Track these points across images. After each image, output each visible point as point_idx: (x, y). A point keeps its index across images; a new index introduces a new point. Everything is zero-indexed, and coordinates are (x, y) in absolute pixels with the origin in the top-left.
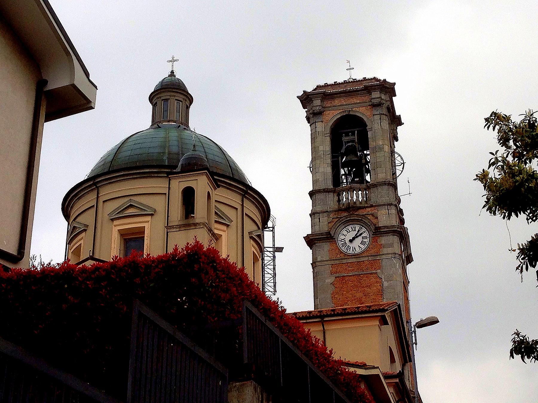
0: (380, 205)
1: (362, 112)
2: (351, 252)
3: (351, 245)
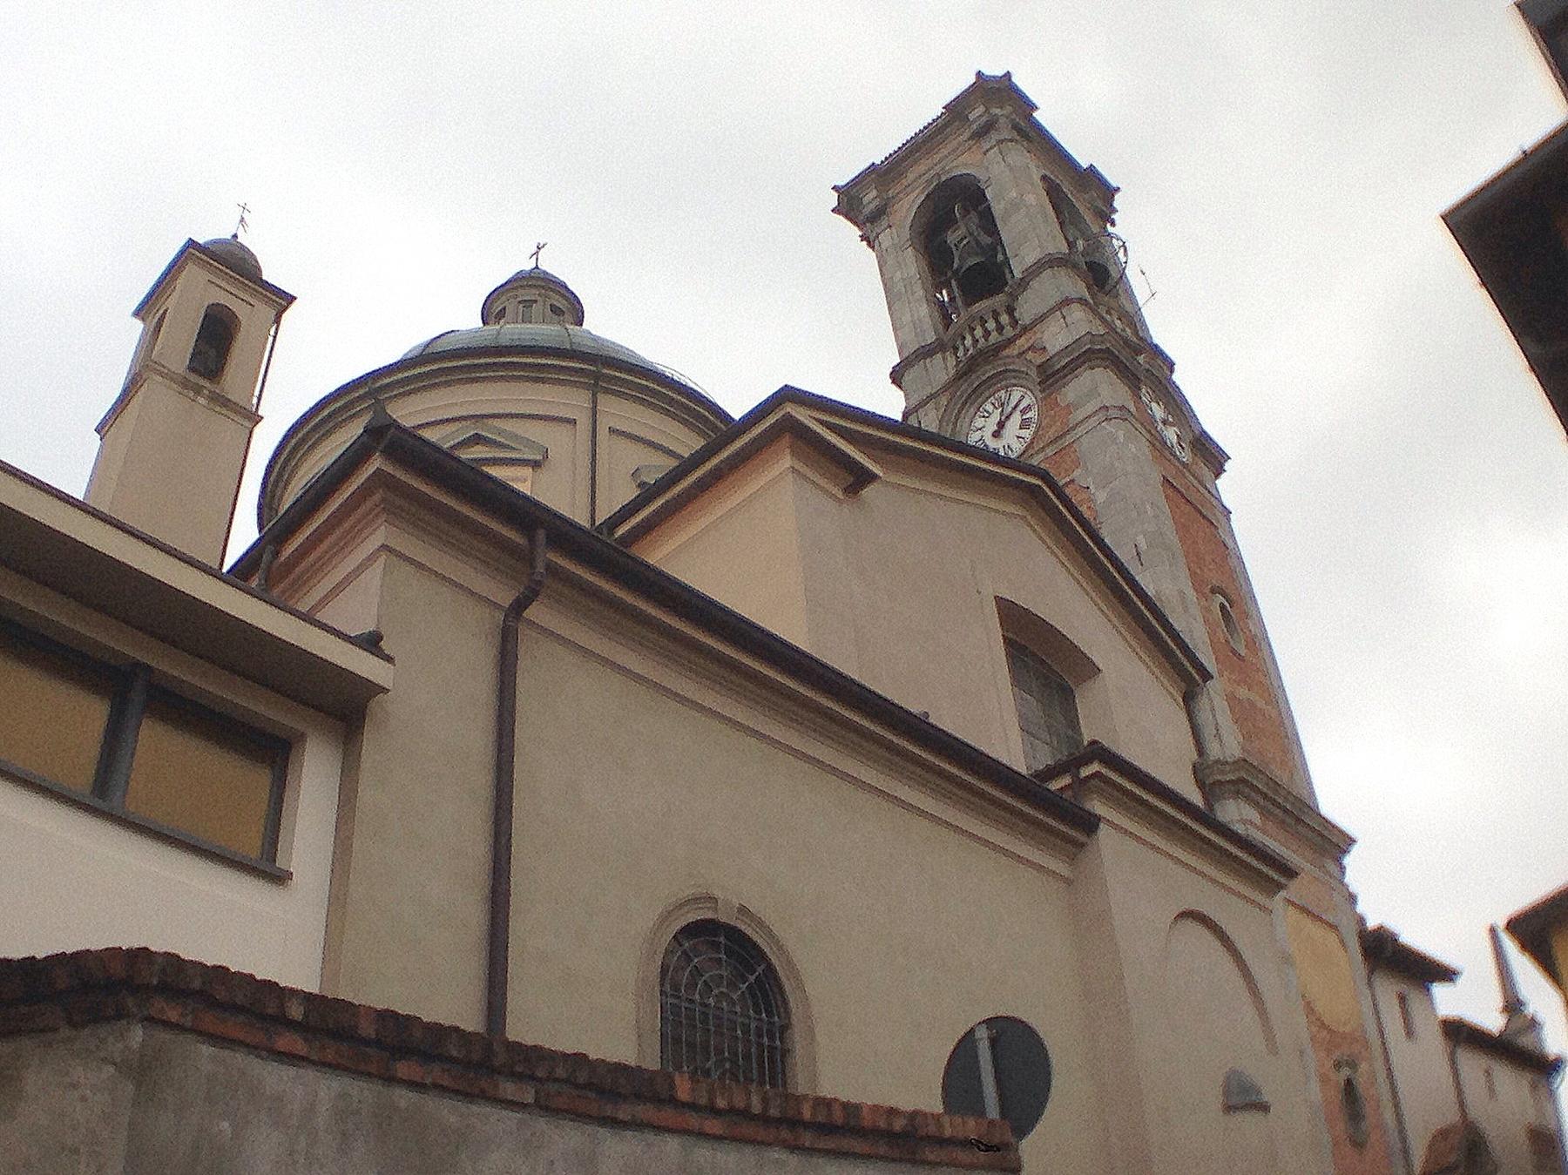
1: (963, 162)
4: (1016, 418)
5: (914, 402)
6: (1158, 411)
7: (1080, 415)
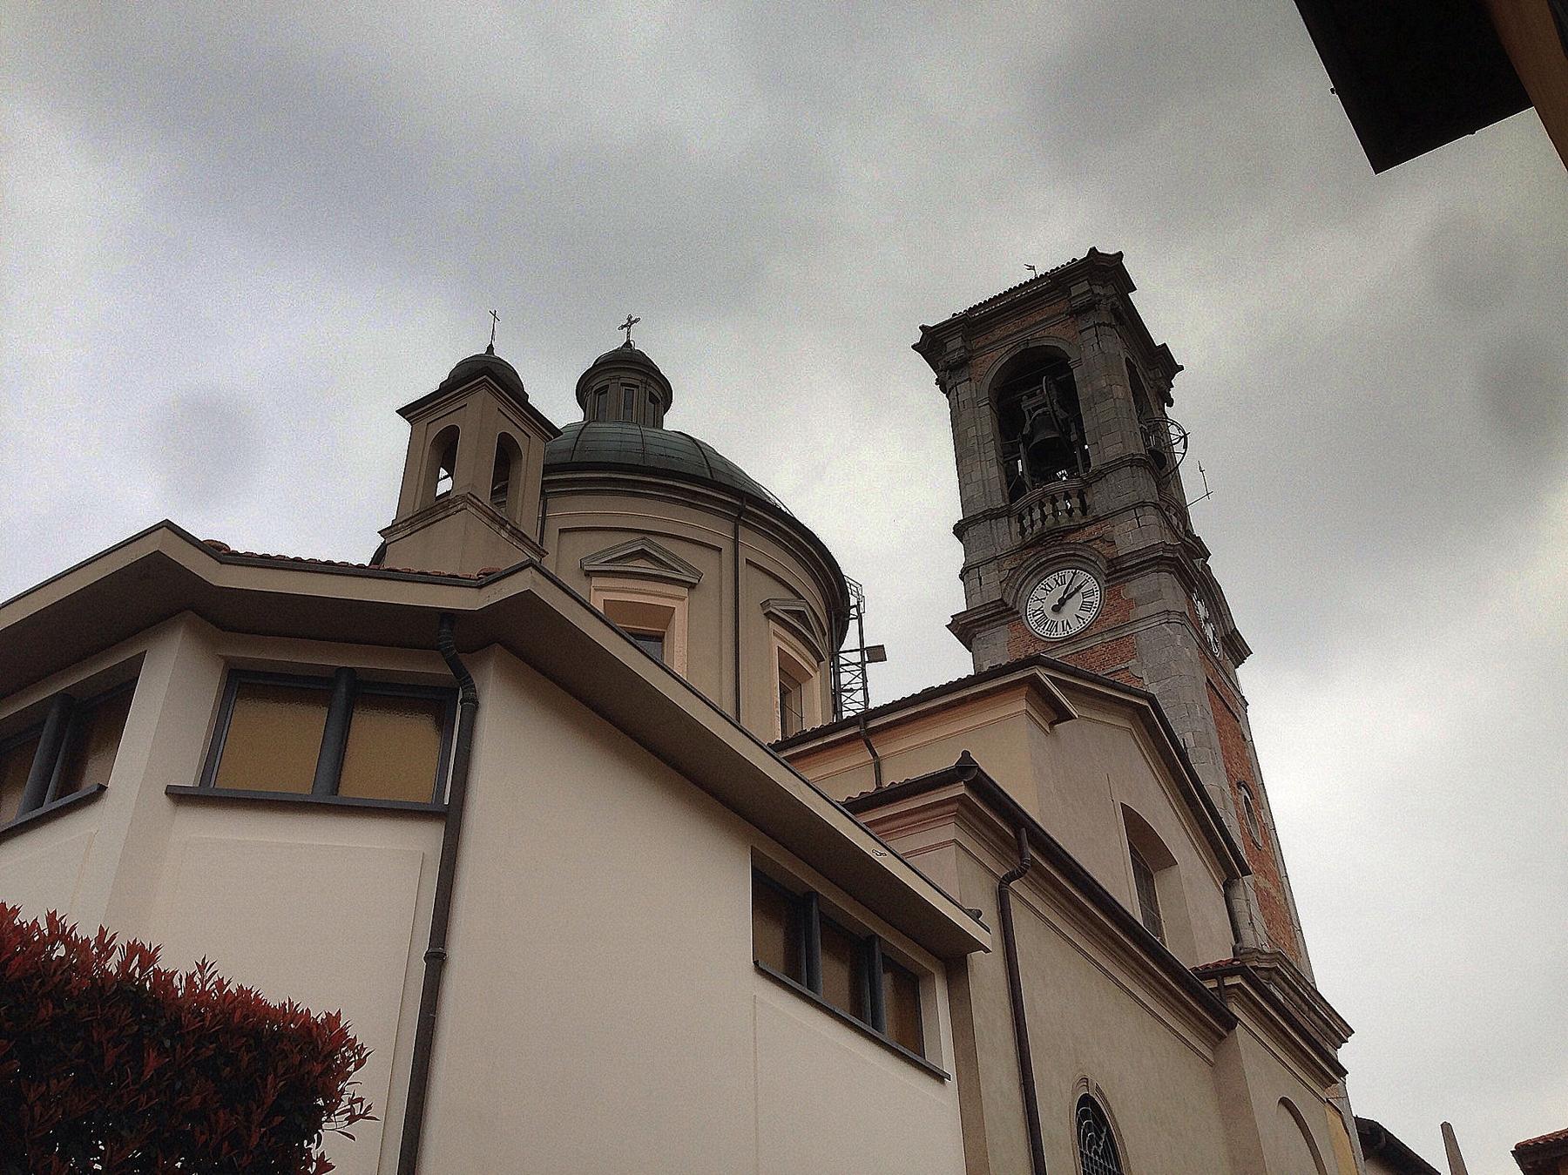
0: (1114, 514)
1: (1053, 333)
2: (1061, 634)
3: (1059, 619)
4: (1077, 600)
5: (975, 560)
6: (1202, 611)
7: (1141, 612)
